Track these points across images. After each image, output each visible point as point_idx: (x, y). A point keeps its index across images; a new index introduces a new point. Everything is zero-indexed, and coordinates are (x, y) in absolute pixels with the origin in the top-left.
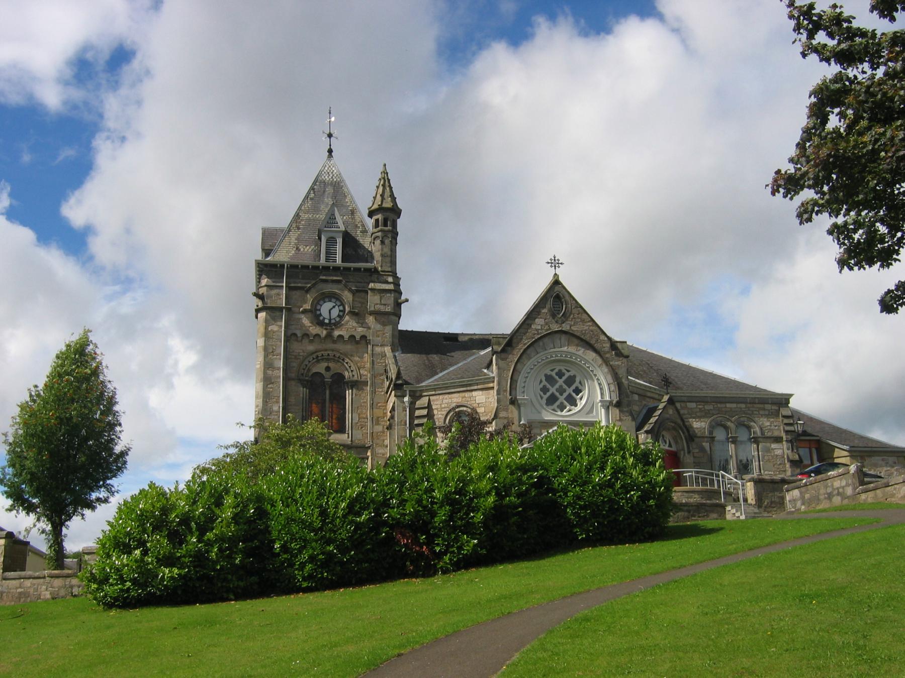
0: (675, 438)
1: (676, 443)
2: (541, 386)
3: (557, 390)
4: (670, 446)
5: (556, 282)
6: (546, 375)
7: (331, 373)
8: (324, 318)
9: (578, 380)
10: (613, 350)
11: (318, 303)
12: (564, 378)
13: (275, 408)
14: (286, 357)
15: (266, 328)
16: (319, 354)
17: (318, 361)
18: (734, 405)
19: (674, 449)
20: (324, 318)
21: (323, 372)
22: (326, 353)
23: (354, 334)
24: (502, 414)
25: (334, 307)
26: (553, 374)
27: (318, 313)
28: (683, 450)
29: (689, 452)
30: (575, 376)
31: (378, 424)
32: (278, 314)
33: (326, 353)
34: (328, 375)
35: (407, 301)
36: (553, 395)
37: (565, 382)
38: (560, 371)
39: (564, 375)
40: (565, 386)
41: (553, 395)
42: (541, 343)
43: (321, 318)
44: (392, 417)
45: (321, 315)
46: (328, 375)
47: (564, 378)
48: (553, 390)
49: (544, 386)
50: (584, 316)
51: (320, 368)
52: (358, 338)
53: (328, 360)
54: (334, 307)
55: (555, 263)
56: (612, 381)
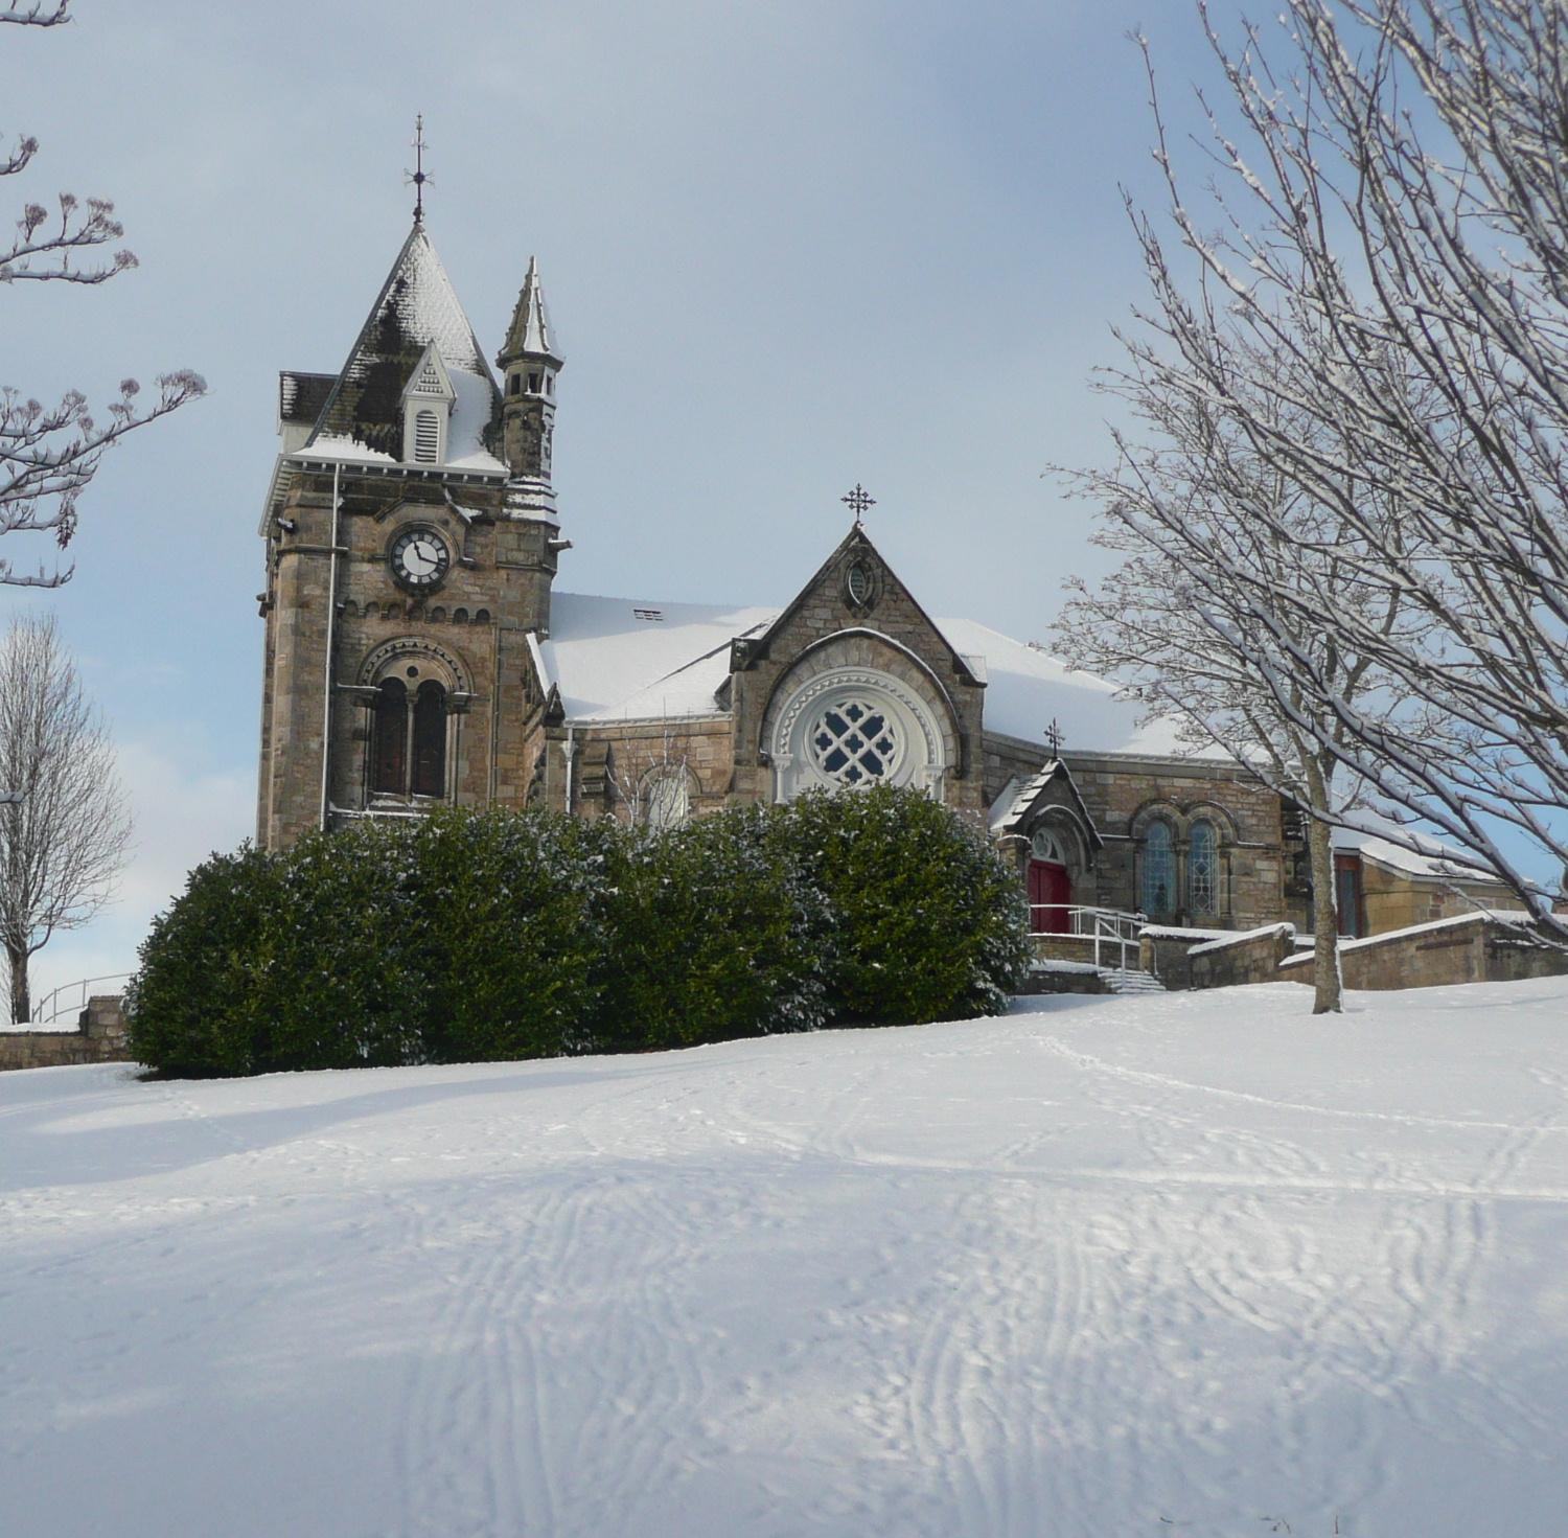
0: (1063, 842)
1: (1066, 849)
2: (890, 753)
3: (861, 745)
4: (1054, 855)
5: (856, 532)
6: (828, 715)
7: (419, 680)
8: (409, 574)
9: (834, 710)
10: (956, 673)
11: (398, 543)
12: (861, 721)
13: (314, 745)
14: (335, 648)
15: (299, 590)
16: (398, 643)
17: (396, 657)
18: (1188, 783)
19: (1061, 861)
20: (409, 574)
21: (404, 678)
22: (409, 642)
23: (465, 606)
24: (744, 785)
25: (417, 548)
26: (823, 755)
27: (398, 562)
28: (1078, 864)
29: (1089, 870)
30: (881, 719)
31: (505, 783)
32: (321, 561)
33: (409, 642)
34: (412, 685)
35: (568, 545)
36: (838, 751)
37: (862, 728)
38: (855, 707)
39: (861, 714)
40: (861, 737)
41: (838, 751)
42: (822, 655)
43: (404, 573)
44: (540, 777)
45: (402, 567)
46: (412, 685)
47: (861, 721)
48: (869, 745)
49: (884, 753)
50: (906, 605)
51: (398, 671)
52: (472, 615)
53: (412, 654)
54: (417, 548)
55: (859, 500)
56: (950, 732)
